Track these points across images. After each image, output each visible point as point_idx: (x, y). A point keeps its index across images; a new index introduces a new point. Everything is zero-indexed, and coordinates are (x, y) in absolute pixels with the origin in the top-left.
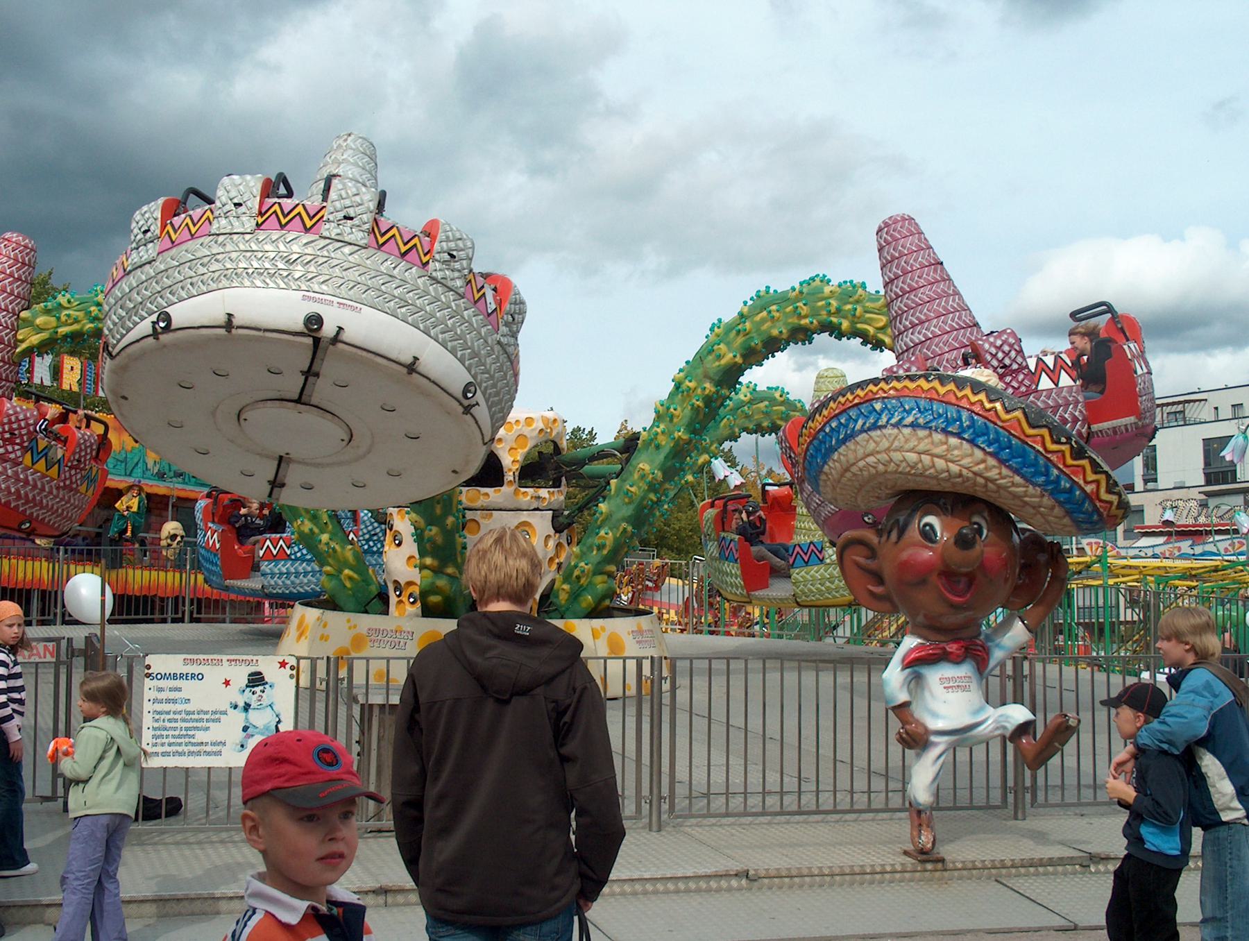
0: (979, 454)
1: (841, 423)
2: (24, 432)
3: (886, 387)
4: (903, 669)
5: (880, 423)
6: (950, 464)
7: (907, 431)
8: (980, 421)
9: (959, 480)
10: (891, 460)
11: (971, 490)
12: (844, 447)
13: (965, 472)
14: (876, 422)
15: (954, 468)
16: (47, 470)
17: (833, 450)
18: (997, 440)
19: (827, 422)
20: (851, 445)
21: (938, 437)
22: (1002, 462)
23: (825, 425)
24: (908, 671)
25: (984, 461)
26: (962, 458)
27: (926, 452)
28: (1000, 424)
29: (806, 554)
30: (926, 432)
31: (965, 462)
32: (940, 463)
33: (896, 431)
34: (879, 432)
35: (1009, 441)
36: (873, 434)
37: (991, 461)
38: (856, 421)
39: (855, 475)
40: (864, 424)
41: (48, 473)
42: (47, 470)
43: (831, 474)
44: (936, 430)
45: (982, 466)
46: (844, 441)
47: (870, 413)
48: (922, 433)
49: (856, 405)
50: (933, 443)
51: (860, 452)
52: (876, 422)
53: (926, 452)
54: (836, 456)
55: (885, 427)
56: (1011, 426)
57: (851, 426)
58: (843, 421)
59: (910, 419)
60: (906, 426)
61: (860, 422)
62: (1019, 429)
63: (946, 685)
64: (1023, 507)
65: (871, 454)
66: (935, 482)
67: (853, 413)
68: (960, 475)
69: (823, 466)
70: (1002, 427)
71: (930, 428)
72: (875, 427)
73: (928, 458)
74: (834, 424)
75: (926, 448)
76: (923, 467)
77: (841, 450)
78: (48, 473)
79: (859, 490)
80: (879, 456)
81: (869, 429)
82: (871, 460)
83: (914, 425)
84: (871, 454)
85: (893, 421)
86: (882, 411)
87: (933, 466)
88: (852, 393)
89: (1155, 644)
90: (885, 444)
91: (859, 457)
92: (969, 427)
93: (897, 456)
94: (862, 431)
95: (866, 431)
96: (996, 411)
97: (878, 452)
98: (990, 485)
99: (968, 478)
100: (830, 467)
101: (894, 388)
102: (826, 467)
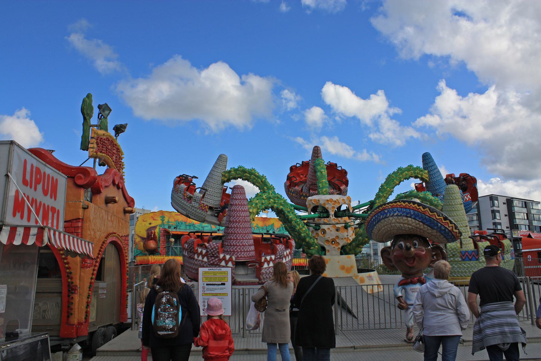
9: (412, 230)
13: (413, 227)
20: (380, 223)
33: (392, 218)
38: (380, 216)
51: (382, 225)
55: (389, 217)
57: (379, 218)
61: (382, 216)
67: (379, 214)
72: (386, 217)
77: (377, 225)
81: (384, 218)
85: (391, 215)
92: (413, 214)
95: (383, 219)
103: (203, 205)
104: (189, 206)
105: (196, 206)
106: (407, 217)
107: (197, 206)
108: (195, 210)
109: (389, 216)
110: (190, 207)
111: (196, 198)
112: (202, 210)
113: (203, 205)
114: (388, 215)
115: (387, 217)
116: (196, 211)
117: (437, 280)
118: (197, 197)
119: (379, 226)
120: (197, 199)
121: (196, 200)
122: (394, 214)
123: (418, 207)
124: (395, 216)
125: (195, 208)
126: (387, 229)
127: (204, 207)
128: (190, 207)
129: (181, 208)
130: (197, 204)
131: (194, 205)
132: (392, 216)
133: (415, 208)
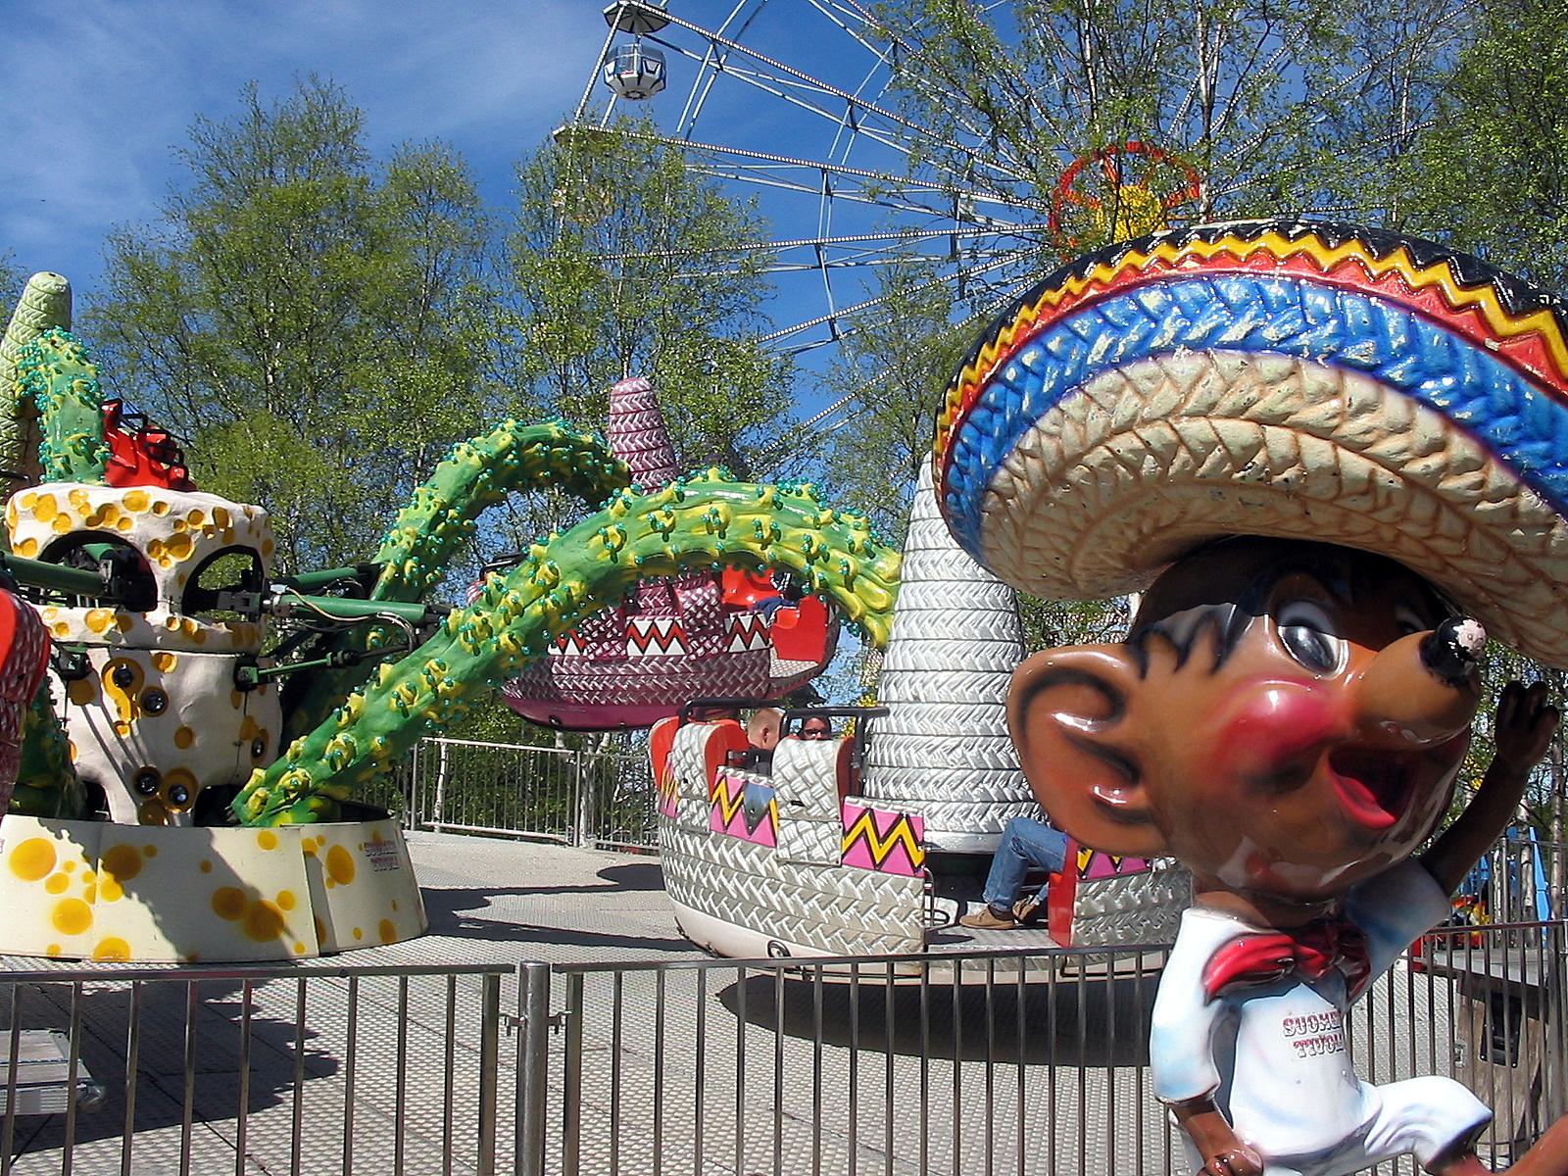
0: (1428, 426)
1: (1049, 353)
2: (609, 624)
3: (1174, 256)
4: (1207, 1003)
5: (1156, 342)
6: (1343, 453)
7: (1231, 360)
8: (1433, 336)
9: (1364, 504)
10: (1181, 441)
11: (1388, 534)
12: (1053, 413)
13: (1384, 476)
14: (1148, 337)
15: (1355, 465)
16: (664, 651)
17: (1026, 422)
18: (1481, 390)
19: (1012, 356)
20: (1072, 404)
21: (1316, 376)
22: (1492, 449)
23: (1004, 365)
24: (1217, 1003)
25: (1438, 446)
26: (1381, 438)
27: (1278, 420)
28: (1494, 345)
29: (881, 840)
30: (1284, 363)
31: (1389, 446)
32: (1317, 452)
33: (1200, 360)
34: (1150, 367)
35: (1516, 390)
36: (1134, 371)
37: (1461, 447)
38: (1089, 342)
39: (1077, 489)
40: (1112, 347)
41: (667, 653)
42: (664, 651)
43: (1014, 493)
44: (1312, 358)
45: (1435, 461)
46: (1053, 399)
47: (1131, 319)
48: (1271, 365)
49: (1092, 303)
50: (1299, 393)
51: (1097, 423)
52: (1148, 337)
53: (1278, 420)
54: (1029, 441)
55: (1168, 351)
56: (1524, 353)
57: (1075, 356)
58: (1053, 345)
59: (1236, 332)
60: (1231, 346)
61: (1102, 342)
62: (1543, 362)
63: (1298, 1038)
64: (1526, 584)
65: (1126, 428)
66: (1292, 508)
67: (1082, 324)
68: (1370, 484)
69: (995, 470)
70: (1499, 355)
71: (1296, 352)
72: (1144, 351)
73: (1286, 434)
74: (1028, 358)
75: (1281, 408)
76: (1269, 459)
77: (1044, 423)
78: (667, 653)
79: (1082, 535)
80: (1147, 433)
81: (1126, 360)
82: (1124, 443)
83: (1249, 345)
84: (1126, 428)
85: (1194, 334)
86: (1164, 311)
87: (1297, 458)
88: (1080, 277)
89: (1390, 826)
90: (1165, 397)
91: (1092, 438)
92: (1405, 351)
93: (1196, 429)
94: (1109, 364)
95: (1115, 366)
96: (1479, 311)
97: (1147, 422)
98: (1447, 519)
99: (1390, 494)
100: (1014, 473)
101: (1198, 257)
102: (1003, 473)
103: (866, 821)
104: (771, 874)
105: (818, 852)
106: (1341, 364)
107: (828, 843)
108: (818, 884)
109: (1176, 339)
110: (779, 871)
111: (798, 785)
112: (877, 867)
113: (866, 821)
114: (1170, 327)
115: (1156, 354)
116: (830, 894)
117: (849, 603)
118: (800, 771)
119: (1068, 429)
120: (810, 786)
121: (804, 798)
122: (1219, 328)
123: (1457, 297)
124: (1231, 346)
125: (819, 866)
126: (1134, 468)
127: (881, 840)
128: (779, 871)
129: (724, 917)
130: (824, 829)
131: (797, 847)
132: (1199, 346)
133: (1430, 294)
